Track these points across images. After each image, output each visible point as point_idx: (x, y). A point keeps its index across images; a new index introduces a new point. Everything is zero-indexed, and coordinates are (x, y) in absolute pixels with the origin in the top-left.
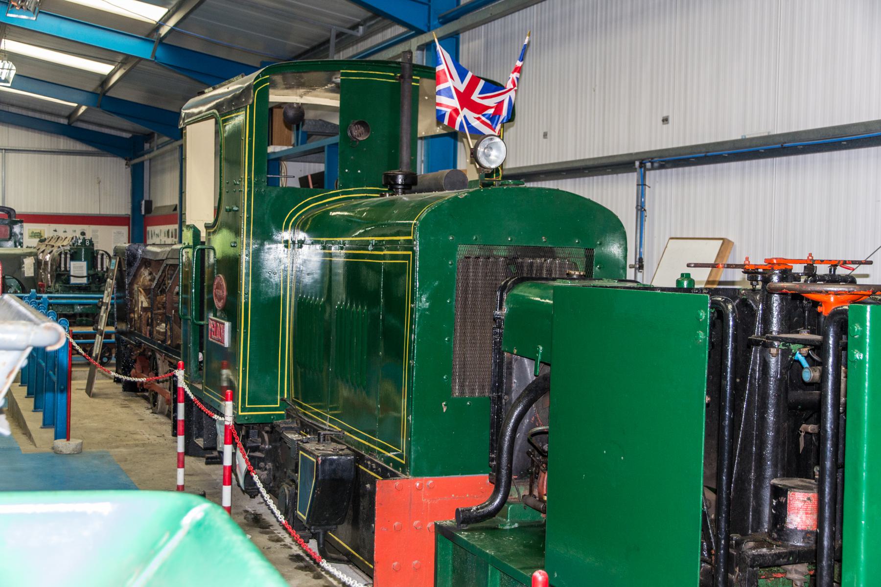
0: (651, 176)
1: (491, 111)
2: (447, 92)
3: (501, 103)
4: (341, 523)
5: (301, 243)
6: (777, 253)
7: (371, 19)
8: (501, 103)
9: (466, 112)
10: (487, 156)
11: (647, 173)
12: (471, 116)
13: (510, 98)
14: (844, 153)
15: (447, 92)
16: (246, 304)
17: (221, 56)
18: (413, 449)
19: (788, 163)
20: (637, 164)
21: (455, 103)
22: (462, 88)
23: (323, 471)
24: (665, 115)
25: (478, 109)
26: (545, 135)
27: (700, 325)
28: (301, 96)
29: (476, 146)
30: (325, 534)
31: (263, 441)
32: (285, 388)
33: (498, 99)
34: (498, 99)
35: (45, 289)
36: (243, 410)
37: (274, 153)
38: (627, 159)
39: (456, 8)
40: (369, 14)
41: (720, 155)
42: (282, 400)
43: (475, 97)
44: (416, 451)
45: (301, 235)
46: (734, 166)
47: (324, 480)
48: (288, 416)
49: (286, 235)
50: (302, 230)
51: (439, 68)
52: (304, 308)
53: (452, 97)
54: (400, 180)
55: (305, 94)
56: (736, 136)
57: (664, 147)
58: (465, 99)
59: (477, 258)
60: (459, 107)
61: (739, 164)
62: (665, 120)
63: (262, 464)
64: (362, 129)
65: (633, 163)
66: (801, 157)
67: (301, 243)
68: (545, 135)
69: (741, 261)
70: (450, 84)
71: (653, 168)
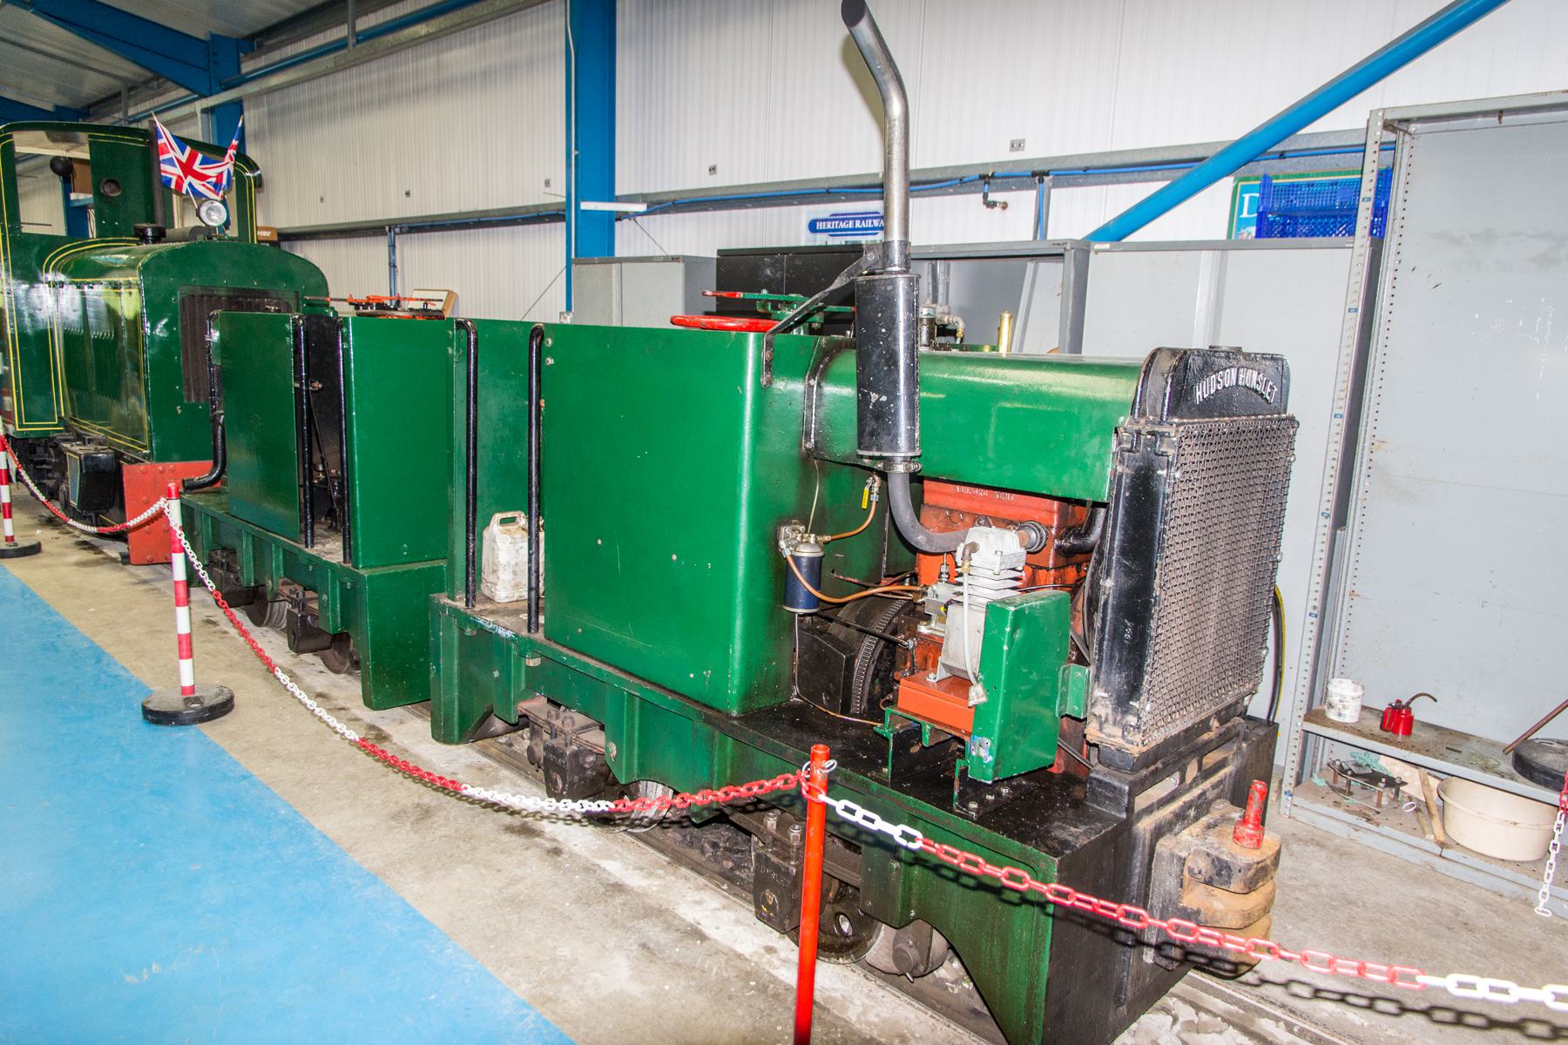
0: (399, 240)
1: (214, 180)
2: (170, 162)
3: (221, 174)
4: (111, 506)
5: (62, 284)
6: (372, 294)
7: (152, 79)
8: (221, 174)
9: (190, 179)
10: (209, 215)
11: (397, 237)
12: (197, 184)
13: (229, 172)
14: (520, 228)
15: (170, 162)
16: (13, 335)
17: (181, 30)
18: (154, 441)
19: (488, 233)
20: (387, 228)
21: (178, 171)
22: (184, 159)
23: (87, 467)
24: (712, 164)
25: (202, 177)
26: (322, 200)
27: (288, 334)
28: (68, 151)
29: (200, 206)
30: (97, 516)
31: (50, 456)
32: (62, 408)
33: (219, 170)
34: (219, 170)
35: (838, 733)
36: (20, 426)
37: (78, 200)
38: (380, 224)
39: (237, 76)
40: (150, 75)
41: (490, 221)
42: (60, 418)
43: (197, 167)
44: (157, 443)
45: (62, 277)
46: (505, 229)
47: (87, 473)
48: (67, 431)
49: (50, 277)
50: (63, 272)
51: (160, 142)
52: (69, 337)
53: (175, 166)
54: (150, 233)
55: (72, 148)
56: (454, 210)
57: (404, 216)
58: (187, 168)
59: (202, 296)
60: (182, 175)
61: (458, 232)
62: (408, 194)
63: (50, 475)
64: (113, 186)
65: (384, 228)
66: (495, 229)
67: (62, 284)
68: (322, 200)
69: (346, 296)
70: (171, 155)
71: (401, 233)
